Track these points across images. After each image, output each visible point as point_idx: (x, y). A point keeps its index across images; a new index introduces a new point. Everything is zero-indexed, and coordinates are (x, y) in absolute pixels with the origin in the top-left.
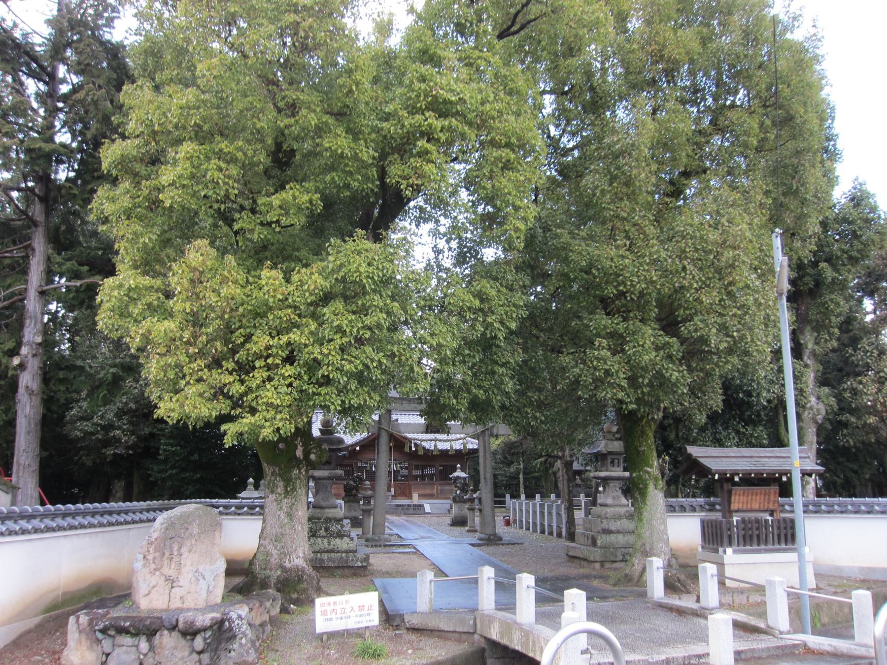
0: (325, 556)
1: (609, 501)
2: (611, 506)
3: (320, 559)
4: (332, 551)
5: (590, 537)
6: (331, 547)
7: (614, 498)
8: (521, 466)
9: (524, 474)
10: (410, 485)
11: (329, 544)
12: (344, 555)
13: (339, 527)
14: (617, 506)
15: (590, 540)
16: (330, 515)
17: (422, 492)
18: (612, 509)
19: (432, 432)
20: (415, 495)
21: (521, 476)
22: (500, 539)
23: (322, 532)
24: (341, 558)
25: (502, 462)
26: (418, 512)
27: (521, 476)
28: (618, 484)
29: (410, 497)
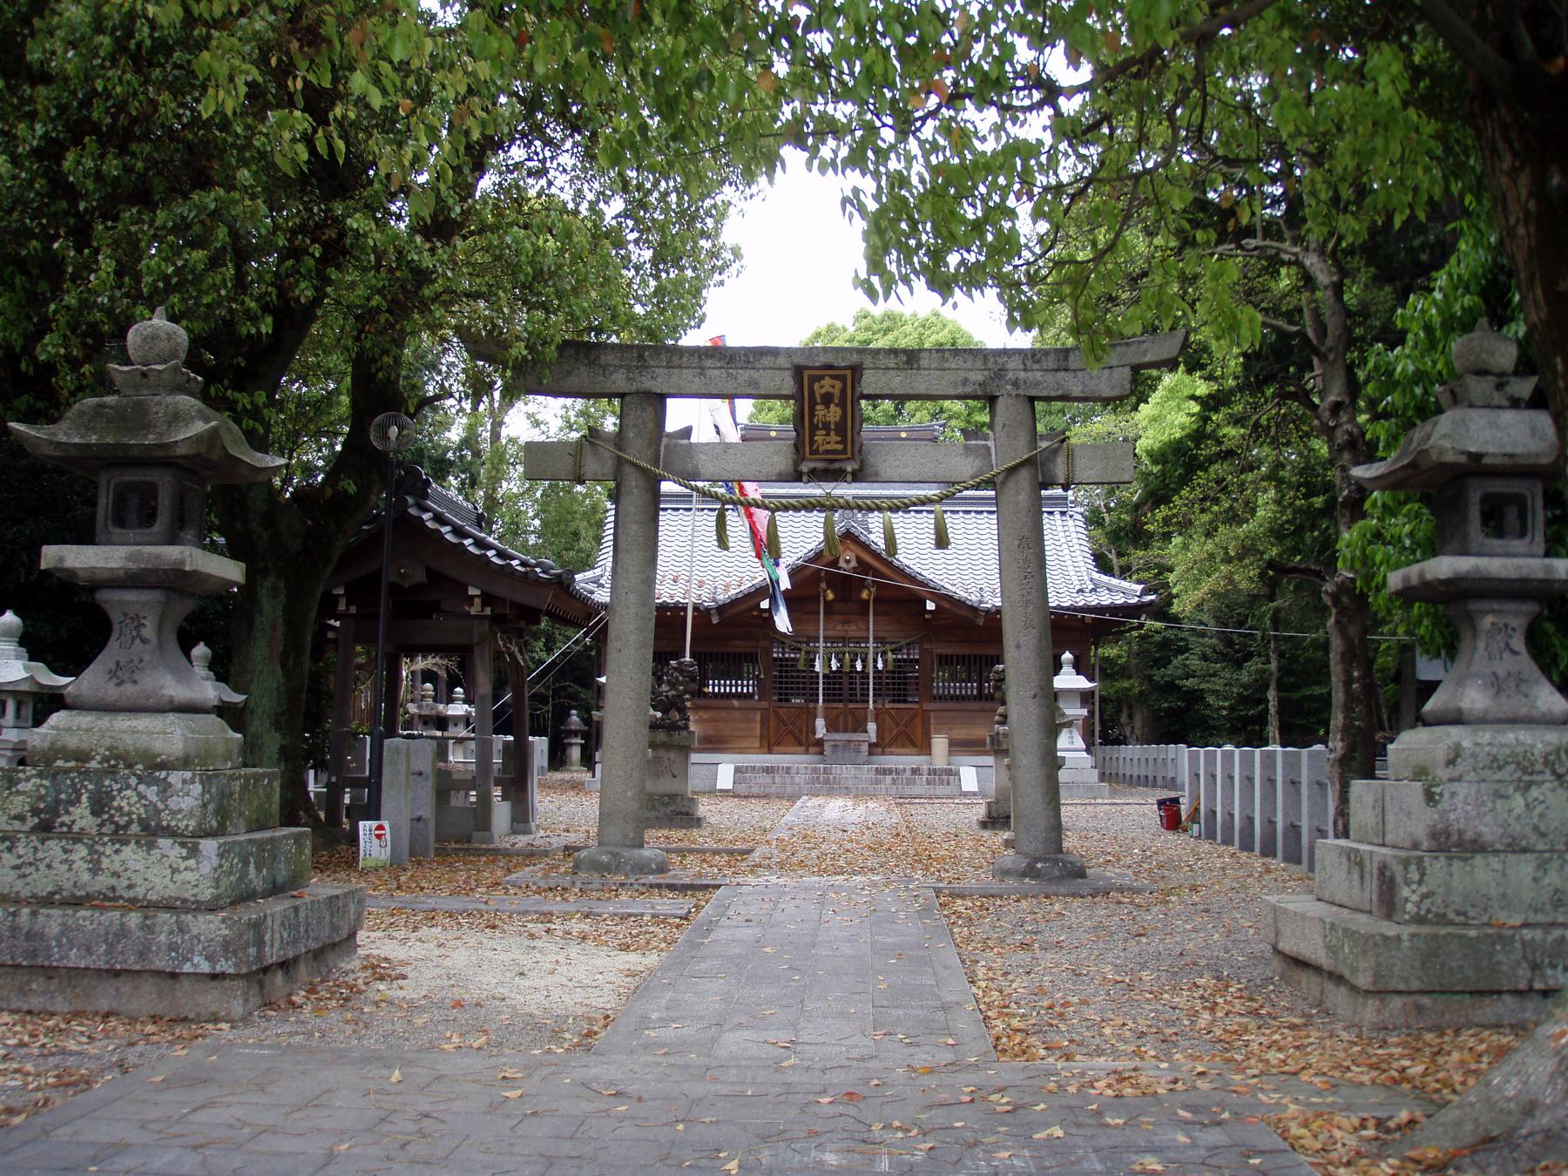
0: (52, 921)
1: (1474, 698)
2: (1482, 721)
3: (31, 936)
4: (104, 900)
5: (1372, 868)
6: (103, 882)
7: (1497, 685)
8: (1273, 666)
9: (1280, 688)
10: (925, 716)
11: (96, 869)
12: (134, 919)
13: (152, 793)
14: (1514, 721)
15: (1373, 885)
16: (129, 742)
17: (961, 733)
18: (1485, 736)
19: (817, 476)
20: (940, 743)
21: (1271, 695)
22: (1080, 873)
23: (81, 816)
24: (123, 932)
25: (1223, 657)
26: (940, 790)
27: (1271, 695)
28: (1516, 617)
29: (925, 748)
